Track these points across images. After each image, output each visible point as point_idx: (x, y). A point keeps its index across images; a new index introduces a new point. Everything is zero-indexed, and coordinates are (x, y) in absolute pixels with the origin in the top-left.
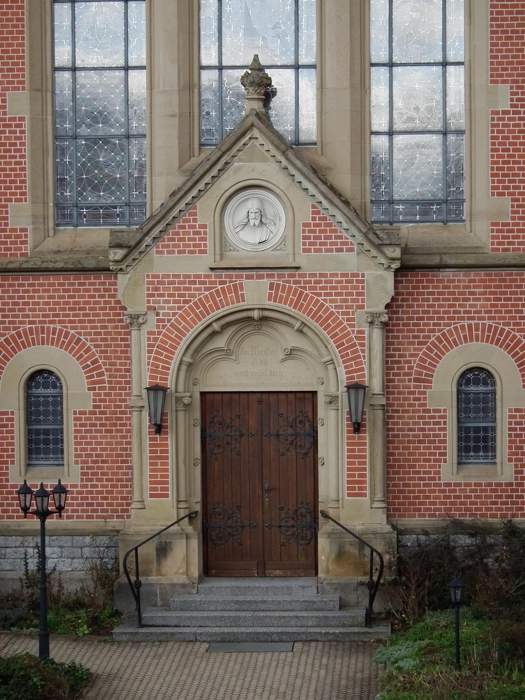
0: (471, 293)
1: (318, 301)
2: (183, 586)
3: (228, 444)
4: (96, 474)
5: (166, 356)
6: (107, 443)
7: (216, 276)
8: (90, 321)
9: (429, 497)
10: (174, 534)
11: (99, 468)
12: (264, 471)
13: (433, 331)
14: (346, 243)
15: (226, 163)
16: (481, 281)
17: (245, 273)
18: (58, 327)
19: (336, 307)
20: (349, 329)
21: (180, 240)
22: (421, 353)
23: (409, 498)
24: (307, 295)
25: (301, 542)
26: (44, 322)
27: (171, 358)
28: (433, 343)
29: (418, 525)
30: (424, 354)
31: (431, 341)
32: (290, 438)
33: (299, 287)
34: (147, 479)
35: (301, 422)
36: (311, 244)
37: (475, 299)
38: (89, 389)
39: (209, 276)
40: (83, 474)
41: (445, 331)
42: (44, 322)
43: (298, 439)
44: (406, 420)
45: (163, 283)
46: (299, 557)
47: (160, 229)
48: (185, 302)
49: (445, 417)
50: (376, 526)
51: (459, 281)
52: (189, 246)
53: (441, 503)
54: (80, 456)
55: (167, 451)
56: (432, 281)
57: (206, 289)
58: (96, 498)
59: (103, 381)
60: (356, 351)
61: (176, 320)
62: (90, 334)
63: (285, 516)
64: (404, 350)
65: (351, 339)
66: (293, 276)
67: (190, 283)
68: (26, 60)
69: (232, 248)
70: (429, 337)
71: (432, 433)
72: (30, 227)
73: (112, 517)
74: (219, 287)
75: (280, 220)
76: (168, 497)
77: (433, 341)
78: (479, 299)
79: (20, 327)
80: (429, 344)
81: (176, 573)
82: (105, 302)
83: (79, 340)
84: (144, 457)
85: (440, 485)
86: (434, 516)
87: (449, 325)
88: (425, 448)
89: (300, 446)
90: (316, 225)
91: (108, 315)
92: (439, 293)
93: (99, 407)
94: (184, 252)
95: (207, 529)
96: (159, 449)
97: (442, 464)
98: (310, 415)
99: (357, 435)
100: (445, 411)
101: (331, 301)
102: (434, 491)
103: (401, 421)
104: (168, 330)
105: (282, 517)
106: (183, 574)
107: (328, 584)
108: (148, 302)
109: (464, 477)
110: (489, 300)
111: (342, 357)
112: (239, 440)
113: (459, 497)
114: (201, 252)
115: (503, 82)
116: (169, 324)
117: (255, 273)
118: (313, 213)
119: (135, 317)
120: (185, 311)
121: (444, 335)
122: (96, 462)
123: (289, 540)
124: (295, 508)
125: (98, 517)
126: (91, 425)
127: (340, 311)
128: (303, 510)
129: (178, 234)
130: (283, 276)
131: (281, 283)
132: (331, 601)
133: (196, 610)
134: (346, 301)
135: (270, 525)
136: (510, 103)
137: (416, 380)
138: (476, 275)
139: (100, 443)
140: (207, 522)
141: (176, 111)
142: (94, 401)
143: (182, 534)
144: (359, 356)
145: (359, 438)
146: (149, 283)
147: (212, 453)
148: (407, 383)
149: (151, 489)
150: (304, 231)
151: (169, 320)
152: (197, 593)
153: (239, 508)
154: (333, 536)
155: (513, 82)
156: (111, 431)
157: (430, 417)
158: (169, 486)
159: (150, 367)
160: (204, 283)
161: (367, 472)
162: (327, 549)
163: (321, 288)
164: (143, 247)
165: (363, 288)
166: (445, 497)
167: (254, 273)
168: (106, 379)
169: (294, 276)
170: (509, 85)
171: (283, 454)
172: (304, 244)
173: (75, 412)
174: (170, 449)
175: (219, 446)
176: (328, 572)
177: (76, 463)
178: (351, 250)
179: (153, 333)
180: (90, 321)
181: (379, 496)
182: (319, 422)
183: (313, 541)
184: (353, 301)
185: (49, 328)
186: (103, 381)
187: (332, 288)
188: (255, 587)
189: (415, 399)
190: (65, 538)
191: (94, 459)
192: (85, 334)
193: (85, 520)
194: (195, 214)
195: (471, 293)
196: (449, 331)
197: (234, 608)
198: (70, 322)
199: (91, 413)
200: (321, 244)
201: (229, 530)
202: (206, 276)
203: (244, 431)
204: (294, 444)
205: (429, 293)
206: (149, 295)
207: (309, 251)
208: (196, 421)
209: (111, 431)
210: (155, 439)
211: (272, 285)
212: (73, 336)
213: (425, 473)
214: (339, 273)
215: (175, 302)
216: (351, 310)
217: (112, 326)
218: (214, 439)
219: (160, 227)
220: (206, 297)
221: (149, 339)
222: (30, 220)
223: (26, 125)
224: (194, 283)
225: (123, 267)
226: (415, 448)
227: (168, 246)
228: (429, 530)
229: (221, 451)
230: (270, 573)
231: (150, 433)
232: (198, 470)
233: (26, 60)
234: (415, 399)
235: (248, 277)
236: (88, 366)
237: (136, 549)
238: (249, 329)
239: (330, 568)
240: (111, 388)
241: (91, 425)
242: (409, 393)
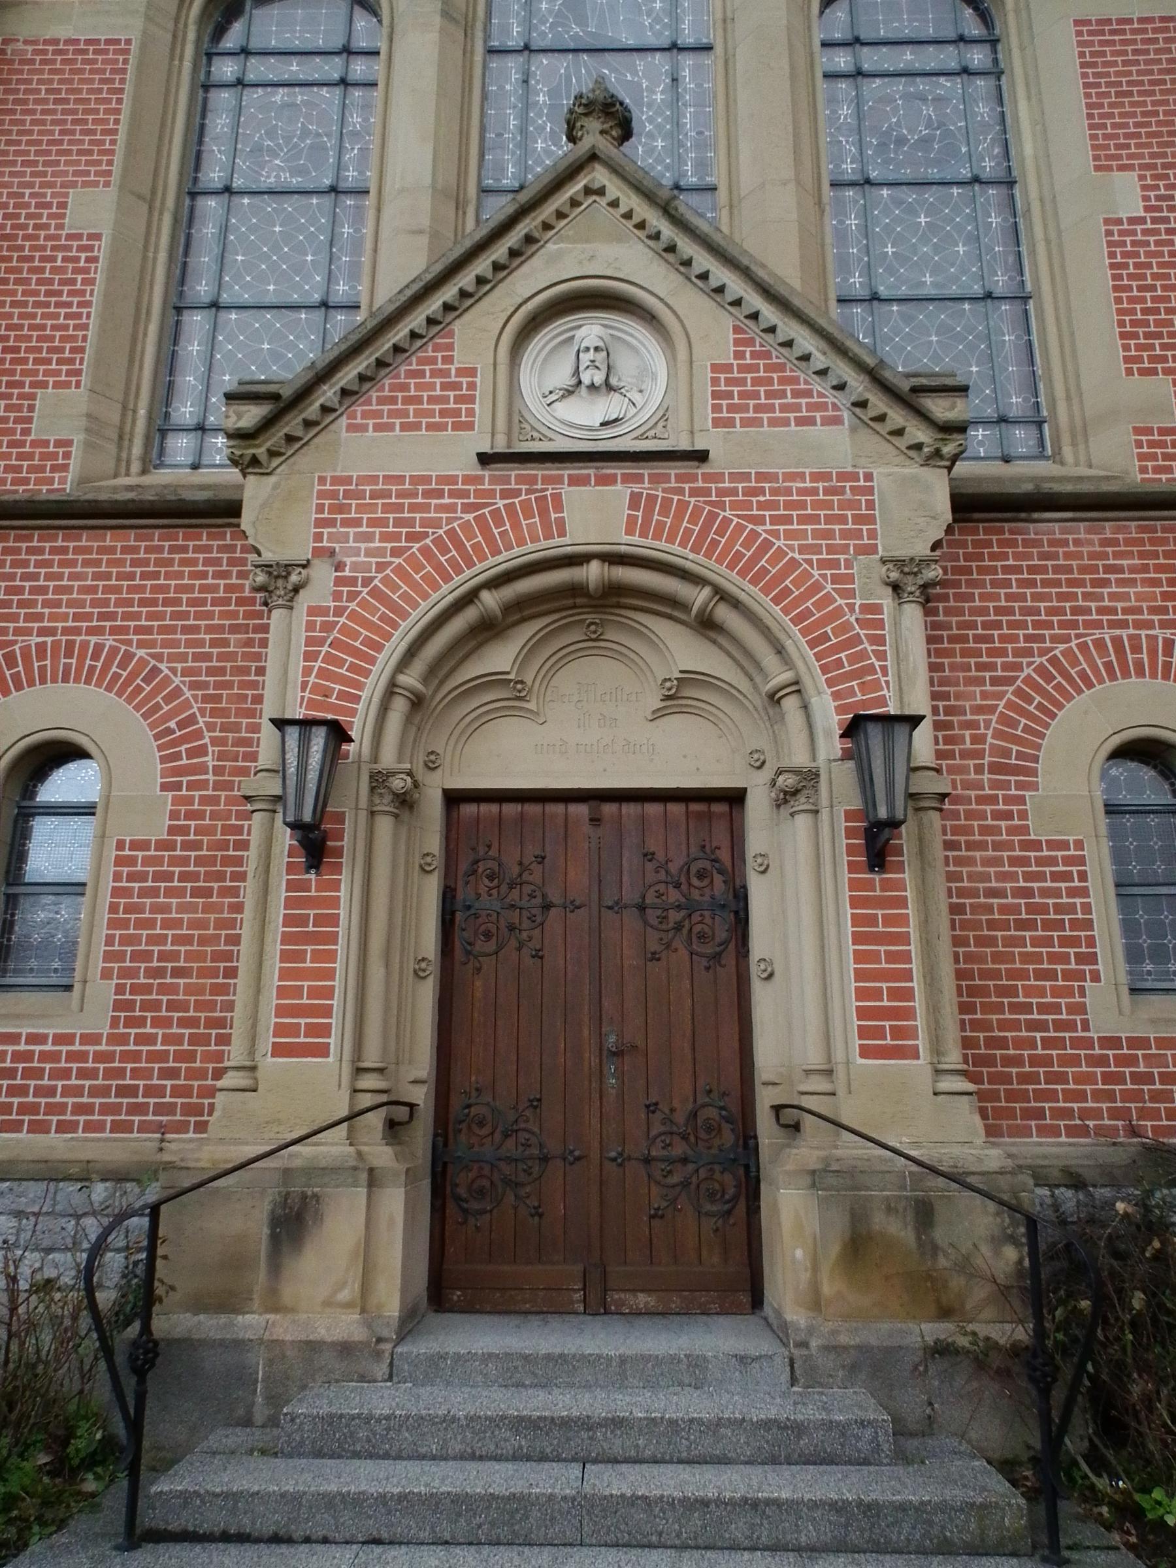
0: (1109, 569)
1: (754, 535)
2: (346, 1349)
3: (512, 928)
4: (155, 1006)
5: (353, 668)
6: (193, 924)
8: (186, 630)
9: (1061, 1078)
10: (331, 1171)
11: (164, 989)
12: (605, 1004)
13: (1029, 653)
14: (822, 407)
15: (529, 239)
16: (1128, 542)
18: (109, 641)
19: (803, 549)
20: (840, 601)
22: (1002, 703)
23: (1006, 1079)
24: (726, 521)
25: (708, 1207)
26: (77, 631)
27: (367, 673)
28: (1028, 680)
29: (1045, 1157)
30: (1010, 705)
31: (1023, 675)
32: (675, 916)
33: (705, 502)
34: (271, 1000)
35: (701, 875)
36: (732, 408)
37: (1121, 583)
38: (165, 787)
39: (478, 480)
40: (119, 1006)
41: (1057, 652)
42: (77, 631)
43: (696, 917)
44: (980, 869)
45: (360, 495)
46: (704, 1253)
47: (360, 369)
49: (1081, 861)
50: (956, 1151)
51: (1077, 542)
52: (430, 413)
53: (1098, 1095)
54: (119, 956)
55: (334, 920)
56: (1012, 543)
57: (467, 508)
58: (146, 1074)
59: (203, 769)
60: (863, 655)
61: (386, 581)
62: (183, 658)
63: (662, 1129)
64: (958, 696)
65: (846, 627)
67: (428, 494)
68: (121, 137)
69: (536, 435)
70: (1018, 667)
71: (1051, 901)
72: (78, 438)
73: (182, 1127)
74: (501, 503)
75: (654, 377)
76: (327, 1055)
77: (1029, 676)
78: (1132, 583)
79: (16, 642)
80: (1018, 682)
81: (328, 1303)
82: (229, 588)
83: (155, 671)
84: (269, 939)
85: (1088, 1043)
86: (1083, 1131)
87: (1067, 639)
88: (1036, 942)
89: (702, 936)
90: (743, 369)
91: (234, 615)
92: (1032, 569)
93: (184, 830)
94: (416, 426)
95: (445, 1164)
96: (312, 912)
97: (1088, 984)
98: (724, 855)
99: (877, 877)
100: (1079, 845)
101: (789, 535)
102: (1075, 1061)
103: (965, 870)
104: (364, 604)
105: (653, 1133)
106: (349, 1305)
107: (827, 1349)
108: (318, 537)
109: (1153, 1021)
110: (1156, 583)
111: (825, 669)
112: (539, 919)
113: (1147, 1078)
114: (457, 427)
115: (1122, 168)
116: (366, 590)
117: (592, 472)
118: (737, 342)
119: (279, 571)
120: (412, 560)
121: (1054, 661)
122: (159, 973)
123: (674, 1201)
124: (690, 1106)
125: (144, 1127)
126: (159, 877)
127: (815, 557)
128: (712, 1113)
129: (404, 387)
131: (660, 494)
132: (862, 1424)
133: (370, 1456)
134: (828, 534)
135: (621, 1154)
136: (1107, 261)
137: (995, 768)
138: (1118, 530)
139: (177, 924)
140: (446, 1144)
141: (425, 222)
143: (355, 1168)
144: (871, 669)
145: (886, 885)
146: (322, 495)
147: (468, 953)
148: (973, 776)
149: (280, 1030)
150: (715, 382)
151: (367, 582)
152: (390, 1379)
153: (536, 1104)
154: (832, 1180)
155: (1143, 167)
156: (208, 893)
158: (333, 1021)
159: (307, 694)
160: (464, 494)
161: (916, 984)
162: (813, 1225)
163: (761, 506)
164: (312, 410)
165: (870, 505)
166: (1108, 1078)
168: (210, 764)
170: (1135, 175)
171: (655, 957)
172: (716, 408)
173: (120, 845)
174: (343, 913)
175: (488, 935)
176: (816, 1303)
177: (106, 974)
179: (323, 611)
180: (186, 630)
181: (954, 1058)
182: (750, 862)
183: (741, 1207)
185: (84, 645)
186: (203, 769)
188: (584, 1358)
189: (998, 815)
190: (35, 1189)
191: (155, 964)
192: (172, 658)
193: (107, 1135)
194: (450, 347)
195: (1109, 569)
196: (1068, 653)
197: (508, 1448)
198: (139, 630)
199: (163, 845)
201: (507, 1169)
202: (468, 480)
203: (555, 897)
204: (685, 931)
205: (1007, 569)
206: (320, 523)
207: (730, 423)
208: (429, 859)
209: (208, 893)
210: (304, 886)
212: (142, 662)
213: (1044, 1008)
214: (807, 471)
215: (385, 537)
216: (842, 557)
217: (237, 641)
218: (476, 916)
219: (361, 365)
220: (466, 526)
221: (310, 626)
222: (83, 422)
223: (102, 250)
225: (261, 452)
226: (1011, 942)
227: (378, 414)
228: (1088, 1175)
229: (491, 946)
230: (622, 1303)
231: (291, 868)
232: (427, 995)
233: (121, 137)
234: (998, 815)
235: (574, 481)
236: (170, 731)
237: (154, 1211)
238: (576, 635)
239: (827, 1289)
240: (218, 786)
241: (159, 877)
242: (981, 800)
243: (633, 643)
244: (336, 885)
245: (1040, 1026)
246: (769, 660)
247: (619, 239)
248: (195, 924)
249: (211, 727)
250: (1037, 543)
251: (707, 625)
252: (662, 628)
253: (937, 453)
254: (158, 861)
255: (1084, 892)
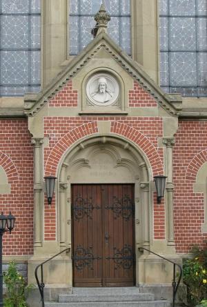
7: (83, 118)
13: (196, 152)
14: (153, 102)
17: (98, 117)
19: (147, 136)
21: (63, 99)
27: (57, 163)
38: (9, 182)
48: (66, 132)
57: (77, 125)
59: (17, 178)
66: (124, 119)
83: (4, 155)
85: (200, 235)
91: (20, 142)
94: (65, 105)
98: (130, 197)
101: (145, 132)
104: (56, 147)
114: (73, 105)
118: (135, 85)
119: (38, 140)
121: (201, 154)
126: (10, 202)
130: (119, 119)
134: (153, 132)
142: (12, 189)
146: (45, 122)
157: (195, 198)
164: (42, 102)
167: (103, 117)
169: (125, 119)
178: (155, 105)
181: (172, 239)
184: (156, 132)
187: (145, 125)
200: (139, 102)
207: (133, 105)
210: (48, 207)
211: (112, 123)
215: (60, 132)
221: (45, 152)
224: (71, 122)
225: (32, 112)
235: (100, 119)
241: (10, 202)
243: (113, 152)
244: (54, 207)
245: (192, 231)
246: (140, 159)
247: (108, 58)
248: (19, 213)
249: (18, 169)
250: (200, 126)
251: (127, 150)
252: (117, 149)
253: (176, 114)
254: (9, 199)
255: (202, 204)
